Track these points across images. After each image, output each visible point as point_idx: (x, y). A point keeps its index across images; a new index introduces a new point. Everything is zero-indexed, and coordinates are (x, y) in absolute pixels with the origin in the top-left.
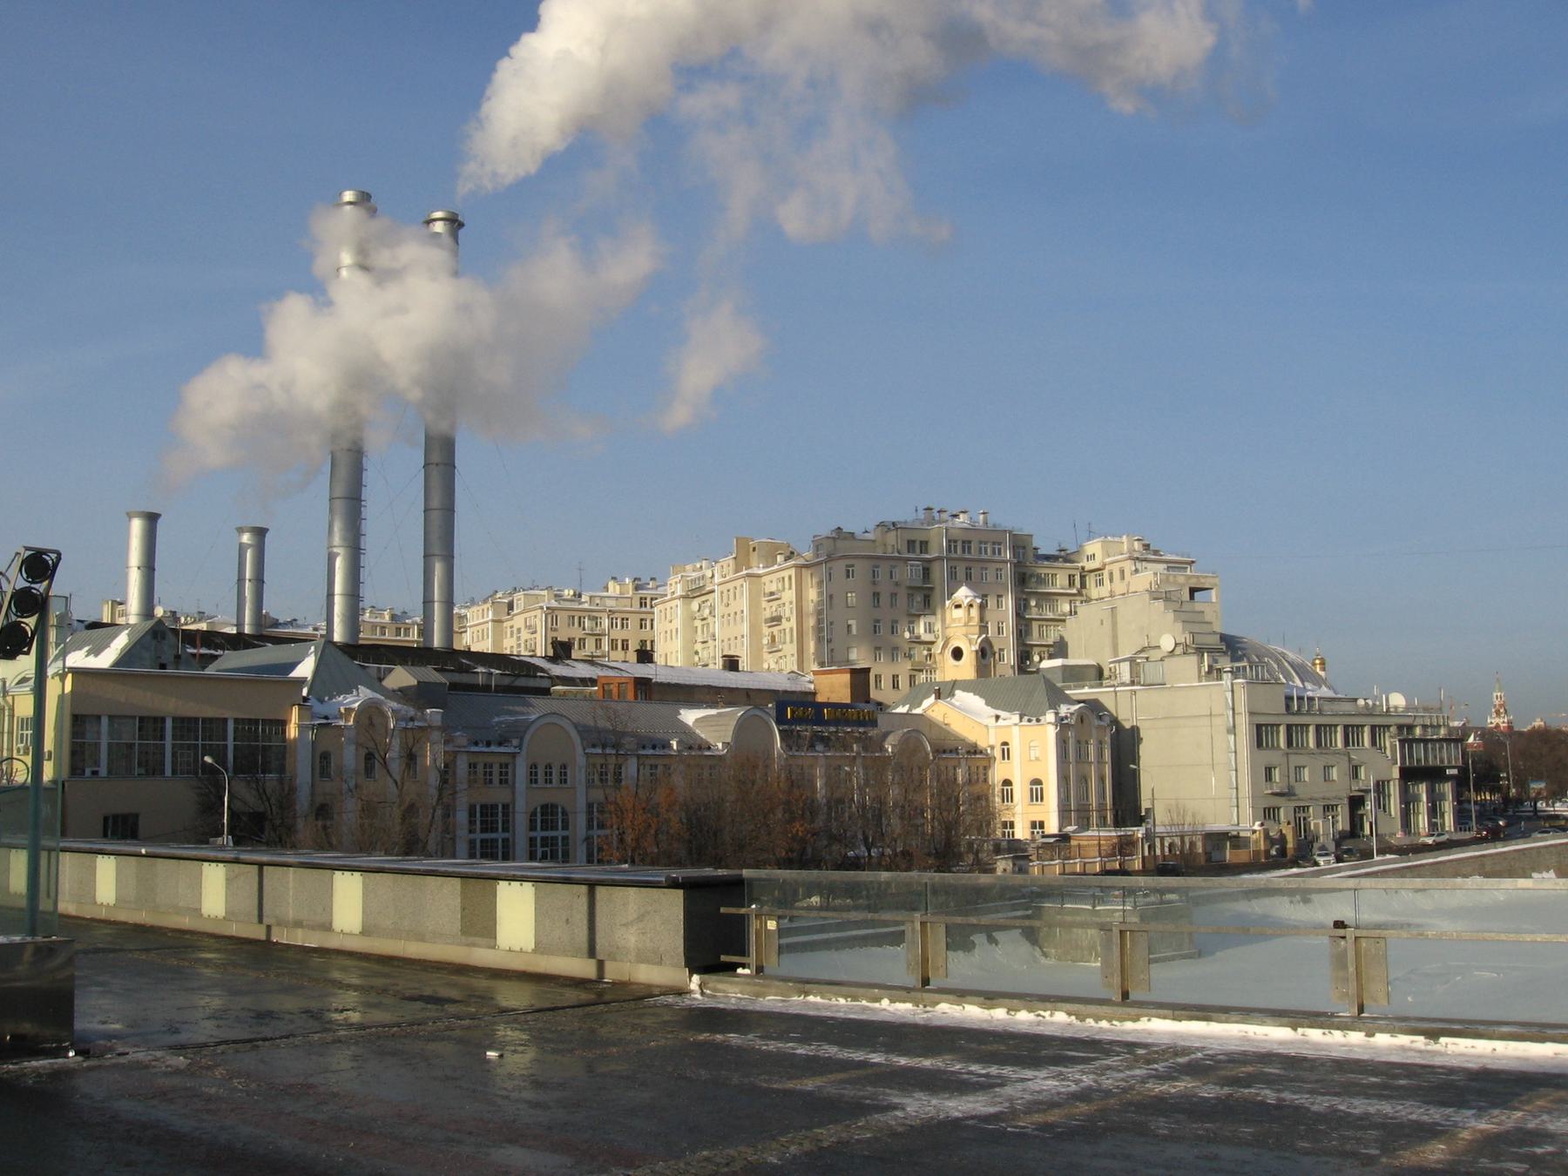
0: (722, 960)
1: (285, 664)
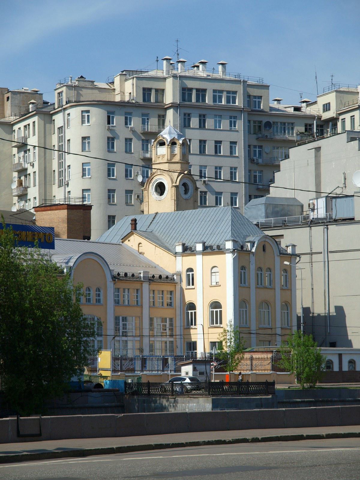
1: (110, 228)
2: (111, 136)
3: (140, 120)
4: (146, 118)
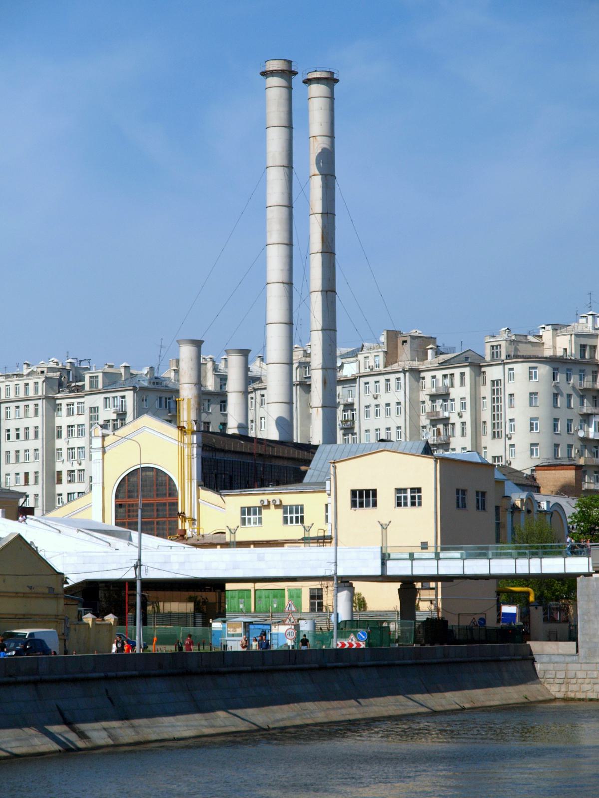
0: (338, 387)
2: (555, 392)
3: (577, 377)
4: (582, 374)
